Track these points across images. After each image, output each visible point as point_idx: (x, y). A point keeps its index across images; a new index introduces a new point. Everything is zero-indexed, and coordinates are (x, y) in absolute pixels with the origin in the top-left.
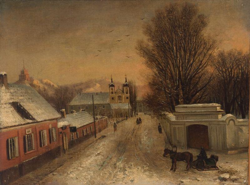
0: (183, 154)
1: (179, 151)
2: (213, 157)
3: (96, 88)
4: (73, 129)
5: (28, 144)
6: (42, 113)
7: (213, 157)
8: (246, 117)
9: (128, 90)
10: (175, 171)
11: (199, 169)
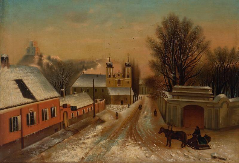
0: (177, 132)
1: (175, 129)
2: (206, 136)
3: (100, 69)
4: (74, 109)
5: (31, 120)
6: (42, 92)
7: (206, 136)
8: (124, 103)
9: (129, 73)
10: (170, 146)
11: (200, 148)
